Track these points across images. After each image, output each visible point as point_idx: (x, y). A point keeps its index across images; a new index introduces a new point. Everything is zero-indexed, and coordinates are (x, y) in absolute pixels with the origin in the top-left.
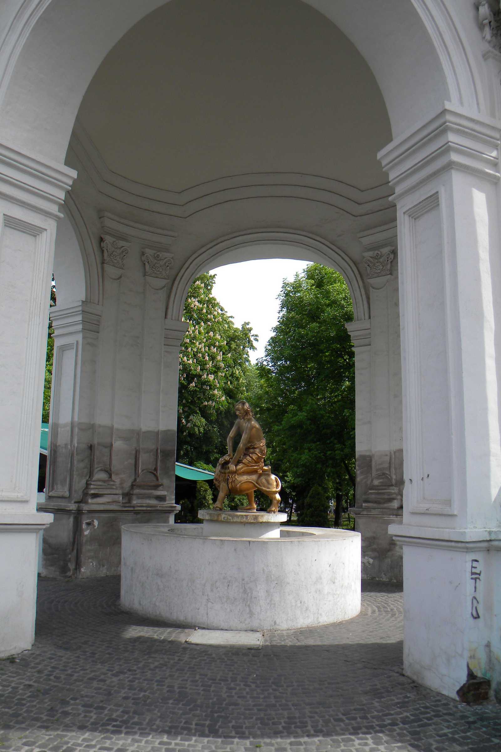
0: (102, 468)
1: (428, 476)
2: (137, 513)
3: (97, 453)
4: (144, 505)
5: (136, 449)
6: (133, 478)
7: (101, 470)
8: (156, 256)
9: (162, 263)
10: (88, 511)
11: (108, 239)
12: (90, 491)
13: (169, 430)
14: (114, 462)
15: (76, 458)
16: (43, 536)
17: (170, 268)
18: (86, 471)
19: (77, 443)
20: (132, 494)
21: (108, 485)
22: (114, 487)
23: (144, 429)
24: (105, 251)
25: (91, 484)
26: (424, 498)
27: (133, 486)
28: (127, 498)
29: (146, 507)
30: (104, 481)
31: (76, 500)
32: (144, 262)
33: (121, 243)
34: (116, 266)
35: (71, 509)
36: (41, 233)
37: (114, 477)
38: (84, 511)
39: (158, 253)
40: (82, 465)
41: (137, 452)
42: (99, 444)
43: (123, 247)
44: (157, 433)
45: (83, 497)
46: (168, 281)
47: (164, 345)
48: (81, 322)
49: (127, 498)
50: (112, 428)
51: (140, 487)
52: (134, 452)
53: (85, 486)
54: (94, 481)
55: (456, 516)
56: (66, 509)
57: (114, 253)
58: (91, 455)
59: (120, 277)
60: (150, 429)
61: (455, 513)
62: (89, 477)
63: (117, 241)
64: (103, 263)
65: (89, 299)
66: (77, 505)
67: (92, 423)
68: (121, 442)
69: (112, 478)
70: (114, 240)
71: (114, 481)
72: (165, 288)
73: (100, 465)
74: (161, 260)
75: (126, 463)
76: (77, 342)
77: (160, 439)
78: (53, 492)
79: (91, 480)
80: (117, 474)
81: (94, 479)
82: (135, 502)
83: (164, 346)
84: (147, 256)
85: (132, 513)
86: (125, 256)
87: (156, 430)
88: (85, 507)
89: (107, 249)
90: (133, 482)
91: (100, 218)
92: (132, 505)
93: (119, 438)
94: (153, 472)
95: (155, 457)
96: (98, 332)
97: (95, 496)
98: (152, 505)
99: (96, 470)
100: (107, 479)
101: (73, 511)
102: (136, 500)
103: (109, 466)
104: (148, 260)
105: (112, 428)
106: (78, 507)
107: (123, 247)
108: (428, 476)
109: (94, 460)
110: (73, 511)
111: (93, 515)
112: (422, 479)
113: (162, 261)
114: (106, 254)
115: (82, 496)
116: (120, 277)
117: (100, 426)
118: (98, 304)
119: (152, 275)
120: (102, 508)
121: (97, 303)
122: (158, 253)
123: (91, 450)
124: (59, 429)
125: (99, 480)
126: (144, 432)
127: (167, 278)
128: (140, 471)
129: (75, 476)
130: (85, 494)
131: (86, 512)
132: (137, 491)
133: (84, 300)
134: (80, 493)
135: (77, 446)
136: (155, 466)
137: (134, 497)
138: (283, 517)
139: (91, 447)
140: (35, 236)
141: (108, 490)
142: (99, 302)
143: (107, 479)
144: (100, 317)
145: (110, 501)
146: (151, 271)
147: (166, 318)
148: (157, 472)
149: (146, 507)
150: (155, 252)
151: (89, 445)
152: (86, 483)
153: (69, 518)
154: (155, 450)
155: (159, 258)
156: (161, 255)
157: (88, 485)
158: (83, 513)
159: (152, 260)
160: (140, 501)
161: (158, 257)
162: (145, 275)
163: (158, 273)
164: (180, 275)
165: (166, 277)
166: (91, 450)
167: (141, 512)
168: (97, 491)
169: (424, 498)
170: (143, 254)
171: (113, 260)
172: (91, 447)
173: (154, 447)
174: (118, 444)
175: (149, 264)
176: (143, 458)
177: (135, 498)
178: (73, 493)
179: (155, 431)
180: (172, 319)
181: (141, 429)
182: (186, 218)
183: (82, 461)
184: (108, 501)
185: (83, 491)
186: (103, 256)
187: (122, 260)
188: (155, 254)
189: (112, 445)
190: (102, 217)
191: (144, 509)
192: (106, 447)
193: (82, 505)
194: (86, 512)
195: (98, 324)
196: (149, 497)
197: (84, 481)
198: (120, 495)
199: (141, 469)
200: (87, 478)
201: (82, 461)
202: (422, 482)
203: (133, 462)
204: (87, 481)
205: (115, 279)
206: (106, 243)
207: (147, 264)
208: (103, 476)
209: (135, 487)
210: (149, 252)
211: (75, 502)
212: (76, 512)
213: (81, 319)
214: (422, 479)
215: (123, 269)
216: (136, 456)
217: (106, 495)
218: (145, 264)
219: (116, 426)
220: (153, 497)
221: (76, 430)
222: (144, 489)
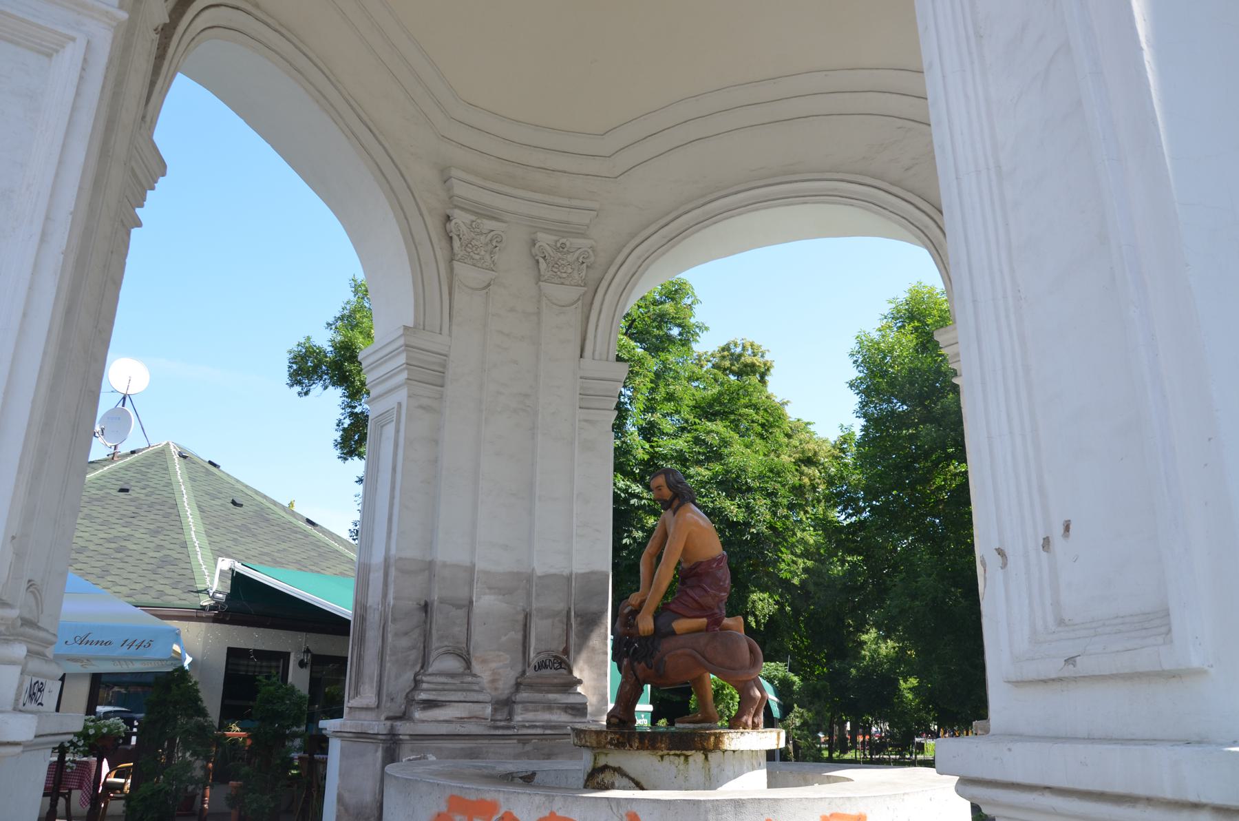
0: (450, 648)
1: (1067, 528)
2: (523, 740)
3: (438, 618)
4: (538, 724)
5: (524, 610)
6: (519, 668)
7: (447, 653)
8: (559, 245)
9: (570, 258)
10: (411, 735)
11: (461, 219)
12: (419, 695)
13: (593, 573)
14: (477, 637)
15: (391, 627)
16: (338, 789)
17: (587, 267)
18: (413, 655)
19: (393, 599)
20: (514, 702)
21: (462, 683)
22: (476, 688)
23: (540, 570)
24: (455, 237)
25: (423, 682)
26: (1061, 622)
27: (518, 686)
28: (506, 710)
29: (543, 727)
30: (452, 675)
31: (391, 714)
32: (537, 258)
33: (488, 224)
34: (480, 265)
35: (376, 732)
36: (63, 47)
37: (477, 667)
38: (401, 737)
39: (564, 240)
40: (404, 642)
41: (527, 617)
42: (442, 601)
43: (493, 231)
44: (569, 578)
45: (406, 708)
46: (586, 289)
47: (580, 408)
48: (405, 366)
49: (506, 710)
50: (471, 569)
51: (531, 687)
52: (521, 617)
53: (413, 685)
54: (430, 675)
55: (1198, 673)
56: (369, 732)
57: (474, 242)
58: (425, 622)
59: (489, 285)
60: (553, 571)
61: (1196, 662)
62: (422, 667)
63: (479, 221)
64: (452, 258)
65: (422, 323)
66: (389, 723)
67: (428, 559)
68: (492, 597)
69: (472, 669)
70: (474, 218)
71: (475, 676)
72: (580, 302)
73: (446, 643)
74: (568, 252)
75: (504, 639)
76: (400, 404)
77: (573, 592)
78: (356, 698)
79: (425, 675)
80: (484, 661)
81: (430, 670)
82: (518, 718)
83: (580, 410)
84: (540, 246)
85: (515, 741)
86: (496, 247)
87: (566, 572)
88: (404, 728)
89: (459, 235)
90: (517, 678)
91: (445, 182)
92: (512, 723)
93: (490, 588)
94: (561, 656)
95: (565, 627)
96: (442, 386)
97: (430, 704)
98: (553, 724)
99: (434, 654)
100: (461, 670)
101: (380, 737)
102: (522, 714)
103: (465, 646)
104: (543, 253)
105: (471, 569)
106: (392, 726)
107: (493, 231)
108: (1067, 528)
109: (430, 632)
110: (380, 737)
111: (426, 743)
112: (1047, 543)
113: (572, 254)
114: (456, 244)
115: (403, 707)
116: (489, 285)
117: (445, 565)
118: (441, 334)
119: (553, 281)
120: (444, 729)
121: (438, 331)
122: (564, 240)
123: (426, 612)
124: (371, 575)
125: (441, 674)
126: (540, 577)
127: (582, 284)
128: (532, 655)
129: (388, 665)
130: (410, 701)
131: (407, 737)
132: (523, 695)
133: (410, 324)
134: (400, 699)
135: (394, 606)
136: (565, 645)
137: (518, 708)
138: (774, 739)
139: (426, 608)
140: (49, 56)
141: (460, 693)
142: (441, 330)
143: (461, 670)
144: (445, 358)
145: (463, 716)
146: (551, 273)
147: (581, 357)
148: (568, 657)
149: (543, 727)
150: (555, 238)
151: (422, 603)
152: (415, 680)
153: (376, 751)
154: (565, 612)
155: (566, 249)
156: (568, 244)
157: (417, 683)
158: (401, 740)
159: (552, 254)
160: (530, 716)
161: (563, 248)
162: (539, 278)
163: (564, 275)
164: (608, 277)
165: (580, 282)
166: (426, 612)
167: (532, 739)
168: (434, 695)
169: (1061, 622)
170: (533, 243)
171: (472, 254)
172: (426, 608)
173: (561, 606)
174: (485, 602)
175: (545, 260)
176: (538, 627)
177: (519, 711)
178: (384, 698)
179: (564, 574)
180: (593, 359)
181: (533, 569)
182: (616, 178)
183: (406, 634)
184: (459, 716)
185: (407, 696)
186: (452, 249)
187: (491, 254)
188: (556, 242)
189: (471, 602)
190: (448, 179)
191: (539, 731)
192: (459, 607)
193: (398, 723)
194: (407, 737)
195: (441, 369)
196: (549, 707)
197: (409, 675)
198: (486, 702)
199: (535, 649)
200: (418, 668)
201: (406, 634)
202: (1044, 554)
203: (520, 636)
204: (416, 675)
205: (477, 289)
206: (456, 223)
207: (541, 260)
208: (453, 664)
209: (522, 687)
210: (545, 239)
211: (388, 719)
212: (389, 737)
213: (404, 362)
214: (1047, 543)
215: (493, 270)
216: (525, 625)
217: (456, 704)
218: (538, 262)
219: (480, 565)
220: (559, 708)
221: (393, 572)
222: (540, 691)
